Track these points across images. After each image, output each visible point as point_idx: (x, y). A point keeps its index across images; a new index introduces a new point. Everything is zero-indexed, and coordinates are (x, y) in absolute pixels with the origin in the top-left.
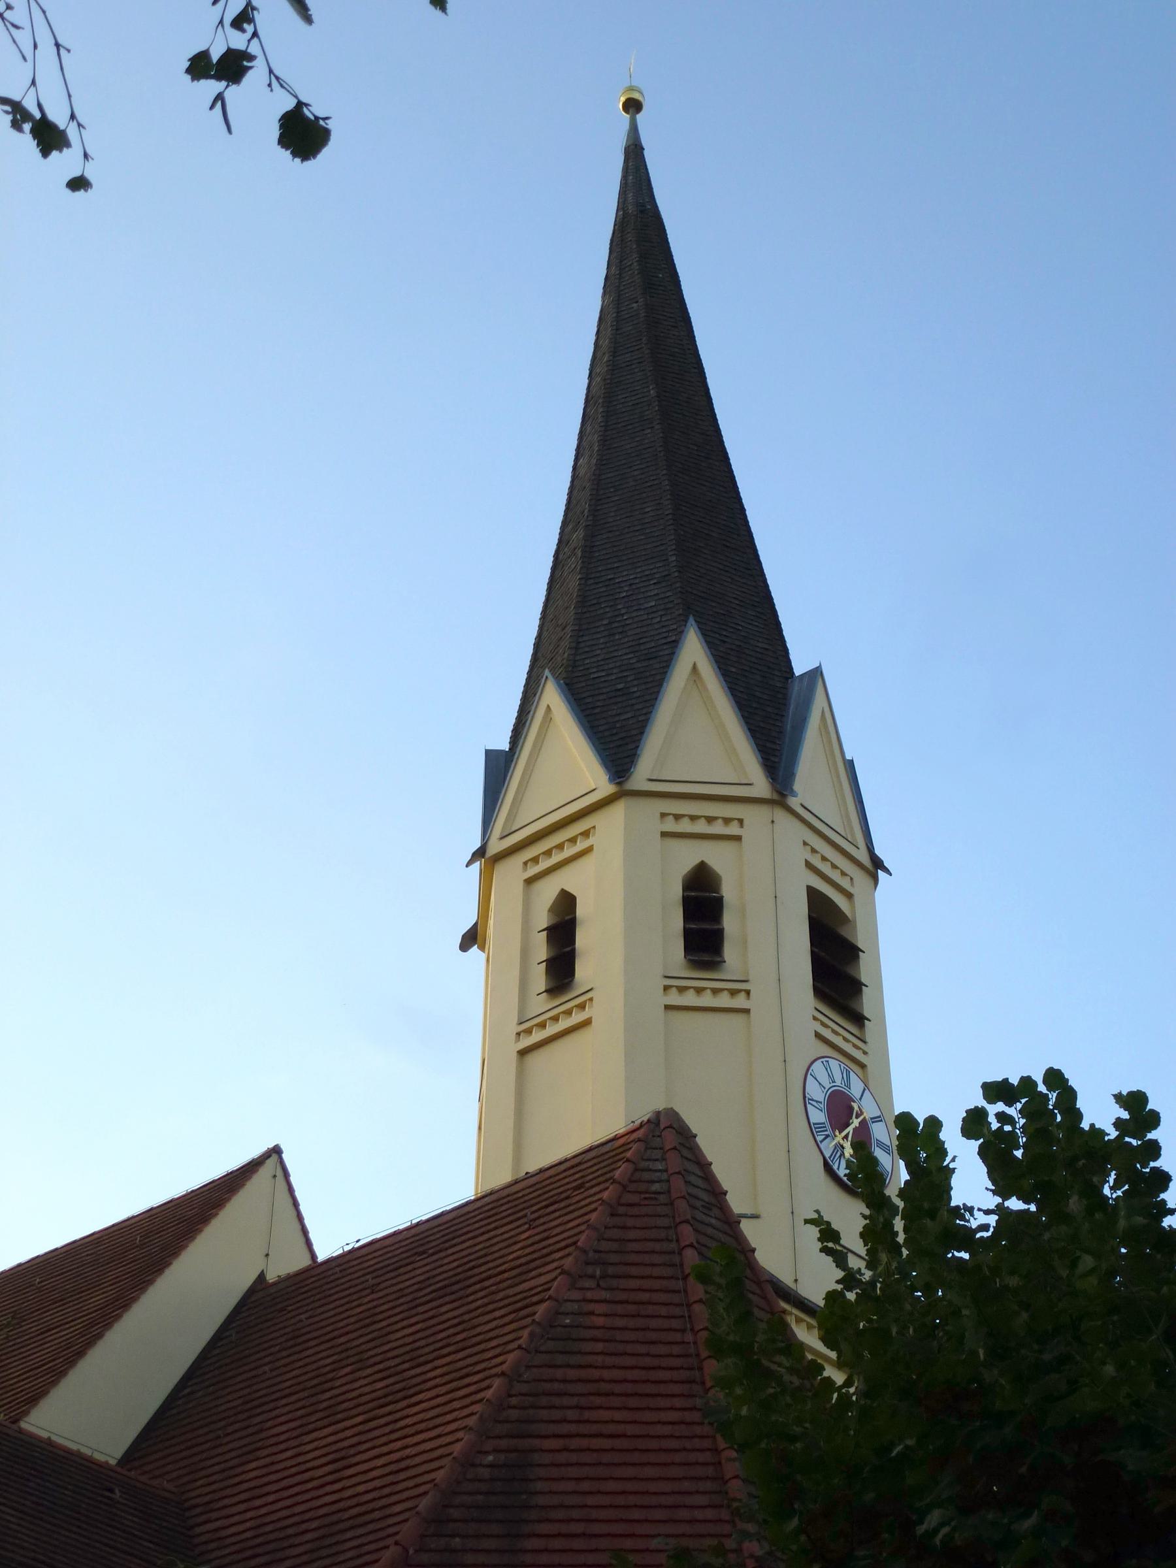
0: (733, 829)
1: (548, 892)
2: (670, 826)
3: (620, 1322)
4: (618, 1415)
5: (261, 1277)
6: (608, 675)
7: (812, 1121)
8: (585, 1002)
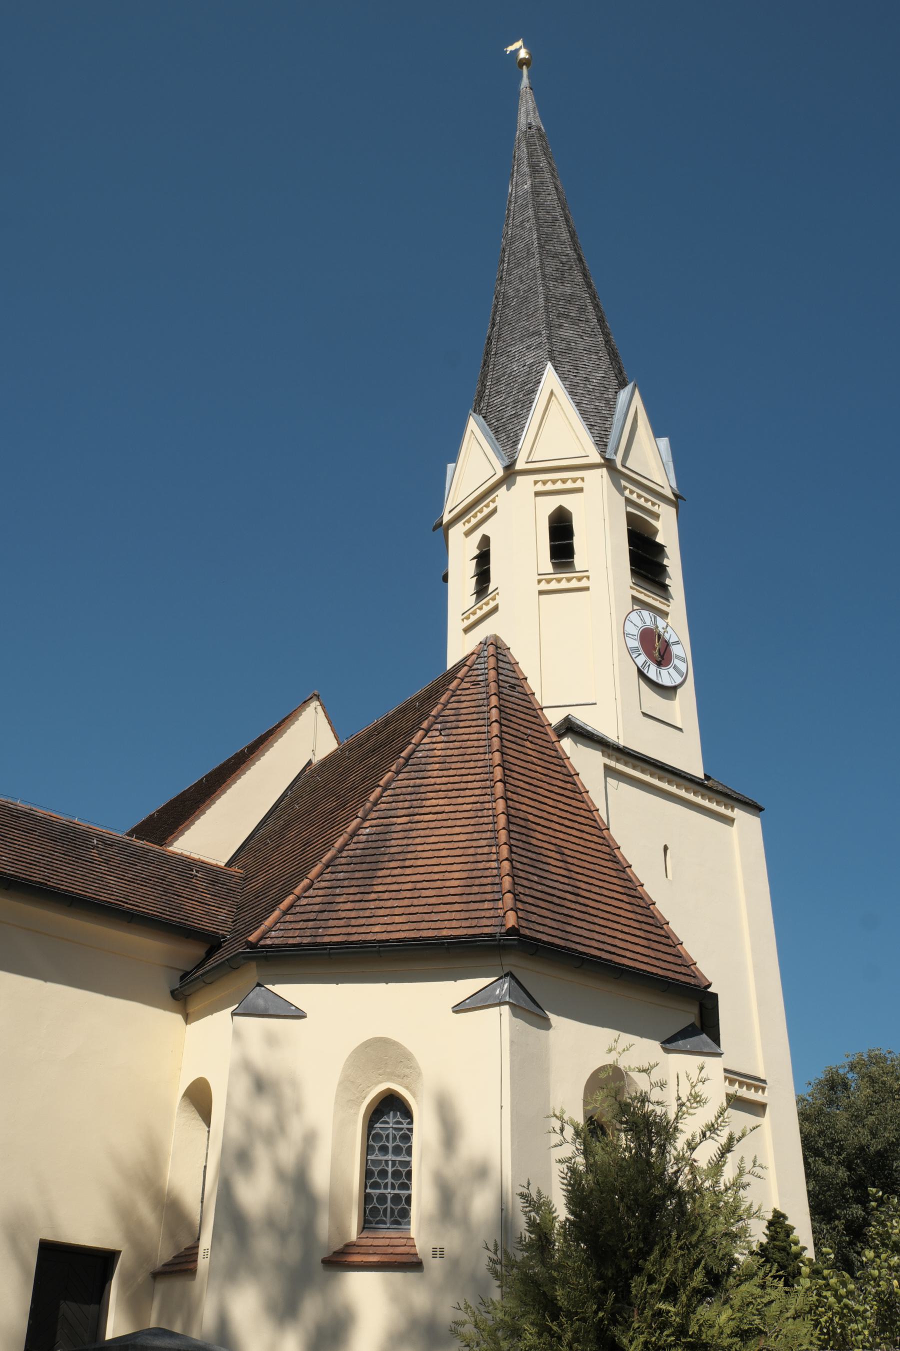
0: (579, 484)
1: (477, 536)
2: (540, 487)
3: (449, 752)
4: (441, 802)
6: (506, 407)
7: (629, 646)
8: (495, 595)
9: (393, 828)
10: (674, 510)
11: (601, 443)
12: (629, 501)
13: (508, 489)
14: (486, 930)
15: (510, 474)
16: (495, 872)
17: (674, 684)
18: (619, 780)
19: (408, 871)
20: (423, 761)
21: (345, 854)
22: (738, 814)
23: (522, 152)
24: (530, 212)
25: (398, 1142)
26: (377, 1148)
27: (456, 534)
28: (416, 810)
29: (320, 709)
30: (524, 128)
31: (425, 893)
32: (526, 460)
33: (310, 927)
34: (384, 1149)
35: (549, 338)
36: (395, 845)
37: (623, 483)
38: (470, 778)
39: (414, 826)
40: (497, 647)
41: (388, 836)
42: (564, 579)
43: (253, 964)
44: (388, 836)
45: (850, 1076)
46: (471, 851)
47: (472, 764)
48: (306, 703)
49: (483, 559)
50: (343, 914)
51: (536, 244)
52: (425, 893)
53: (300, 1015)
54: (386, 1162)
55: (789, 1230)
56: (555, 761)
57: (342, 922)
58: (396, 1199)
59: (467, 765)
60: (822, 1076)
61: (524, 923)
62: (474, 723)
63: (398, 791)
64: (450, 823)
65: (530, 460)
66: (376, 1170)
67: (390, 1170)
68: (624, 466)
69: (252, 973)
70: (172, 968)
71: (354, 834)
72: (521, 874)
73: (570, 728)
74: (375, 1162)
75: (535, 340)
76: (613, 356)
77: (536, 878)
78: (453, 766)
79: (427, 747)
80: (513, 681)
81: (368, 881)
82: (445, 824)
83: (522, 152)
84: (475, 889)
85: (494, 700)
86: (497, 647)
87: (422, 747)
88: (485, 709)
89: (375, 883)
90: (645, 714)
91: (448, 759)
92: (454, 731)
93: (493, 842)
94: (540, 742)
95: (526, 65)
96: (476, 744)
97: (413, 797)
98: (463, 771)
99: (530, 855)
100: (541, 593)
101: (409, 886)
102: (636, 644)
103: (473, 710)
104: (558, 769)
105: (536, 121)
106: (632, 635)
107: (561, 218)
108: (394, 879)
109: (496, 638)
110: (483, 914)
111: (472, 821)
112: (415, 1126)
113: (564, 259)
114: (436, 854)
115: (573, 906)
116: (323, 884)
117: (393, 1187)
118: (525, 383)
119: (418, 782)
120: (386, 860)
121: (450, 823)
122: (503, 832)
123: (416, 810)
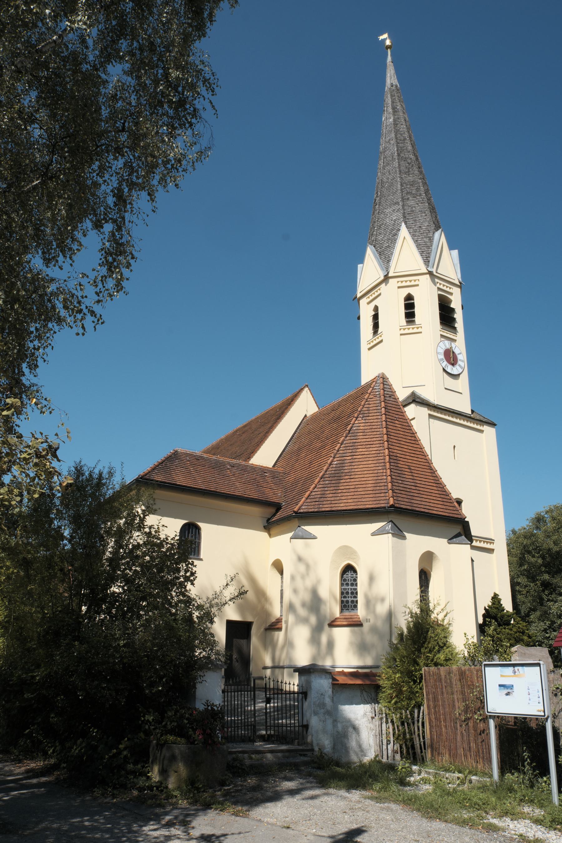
1: (372, 305)
2: (400, 284)
3: (366, 428)
4: (364, 450)
5: (306, 416)
9: (346, 462)
10: (459, 289)
11: (427, 262)
12: (439, 289)
13: (386, 285)
14: (382, 505)
15: (386, 278)
16: (385, 480)
19: (352, 480)
20: (356, 431)
21: (328, 473)
22: (486, 428)
23: (389, 100)
24: (393, 135)
25: (352, 582)
27: (363, 302)
28: (354, 454)
29: (308, 391)
30: (389, 86)
31: (359, 490)
34: (347, 584)
35: (403, 206)
36: (347, 469)
37: (437, 280)
38: (374, 439)
39: (354, 460)
40: (383, 378)
41: (344, 465)
43: (297, 519)
44: (344, 465)
45: (546, 516)
46: (376, 471)
47: (375, 433)
48: (302, 390)
49: (376, 317)
50: (329, 499)
51: (396, 154)
52: (359, 490)
53: (315, 538)
55: (499, 601)
56: (407, 428)
57: (329, 502)
58: (352, 601)
59: (373, 433)
60: (534, 516)
61: (396, 502)
62: (375, 414)
63: (347, 445)
64: (367, 459)
66: (345, 592)
67: (350, 591)
68: (437, 273)
69: (296, 522)
71: (331, 464)
72: (395, 481)
73: (415, 399)
74: (344, 589)
75: (396, 207)
76: (433, 210)
77: (400, 482)
78: (368, 434)
79: (357, 425)
80: (390, 393)
81: (337, 485)
82: (366, 459)
83: (389, 100)
84: (378, 488)
85: (383, 404)
86: (383, 378)
87: (355, 425)
88: (379, 408)
90: (446, 389)
91: (366, 431)
92: (368, 418)
93: (384, 467)
94: (401, 420)
96: (376, 424)
97: (353, 448)
98: (372, 436)
99: (398, 472)
100: (401, 335)
101: (353, 487)
102: (442, 357)
103: (375, 408)
104: (409, 431)
105: (395, 82)
108: (347, 484)
109: (383, 374)
110: (381, 498)
111: (376, 458)
112: (358, 576)
113: (409, 161)
114: (363, 473)
115: (414, 491)
116: (320, 486)
117: (351, 597)
118: (392, 230)
119: (354, 441)
121: (367, 459)
122: (388, 464)
123: (354, 454)
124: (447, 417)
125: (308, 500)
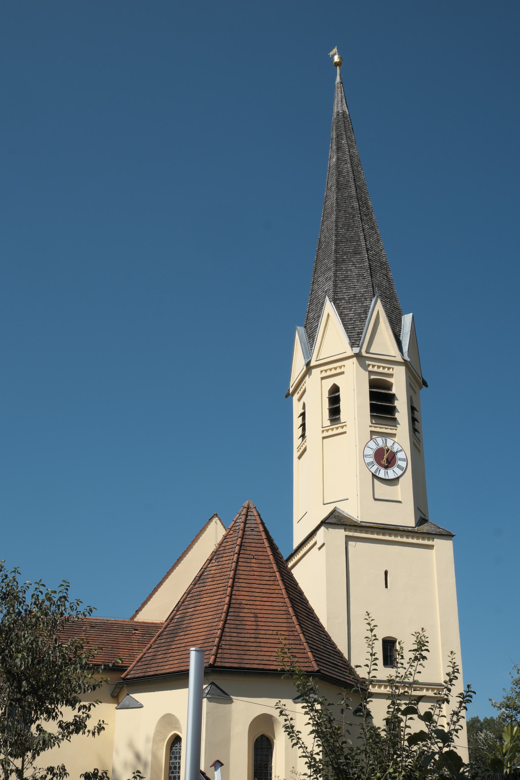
2: (324, 374)
11: (354, 341)
12: (371, 373)
17: (397, 476)
18: (356, 542)
22: (437, 542)
26: (173, 757)
29: (218, 521)
32: (315, 360)
33: (145, 668)
37: (368, 362)
42: (335, 428)
48: (210, 520)
54: (176, 762)
65: (318, 359)
66: (173, 766)
70: (112, 684)
74: (173, 763)
87: (208, 569)
89: (173, 644)
92: (221, 559)
95: (339, 66)
102: (372, 459)
106: (369, 455)
107: (351, 180)
120: (180, 631)
124: (375, 536)
125: (139, 664)
